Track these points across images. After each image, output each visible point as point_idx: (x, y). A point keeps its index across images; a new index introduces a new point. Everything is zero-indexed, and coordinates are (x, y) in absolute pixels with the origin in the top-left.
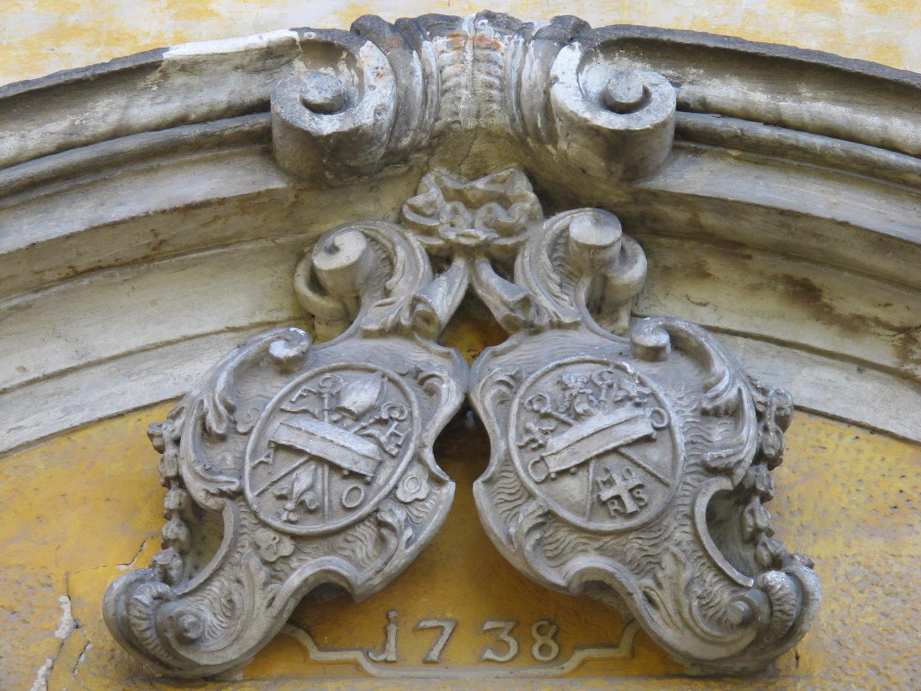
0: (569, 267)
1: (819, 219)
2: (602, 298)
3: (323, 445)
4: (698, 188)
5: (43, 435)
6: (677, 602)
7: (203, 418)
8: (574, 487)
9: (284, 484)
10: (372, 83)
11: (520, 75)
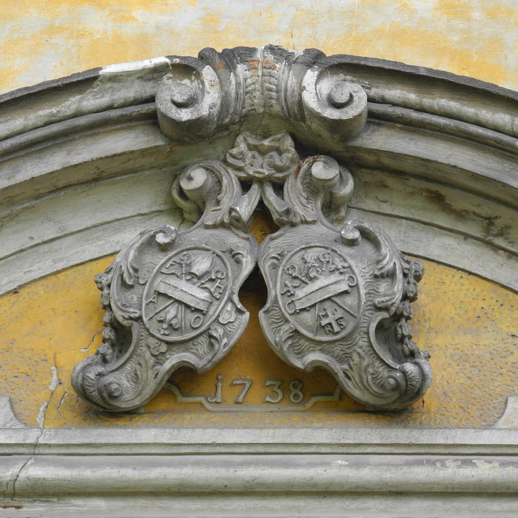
0: (312, 188)
1: (441, 163)
2: (331, 202)
3: (182, 294)
4: (379, 146)
5: (42, 275)
6: (361, 377)
7: (122, 275)
8: (308, 317)
9: (162, 314)
10: (208, 90)
11: (286, 84)
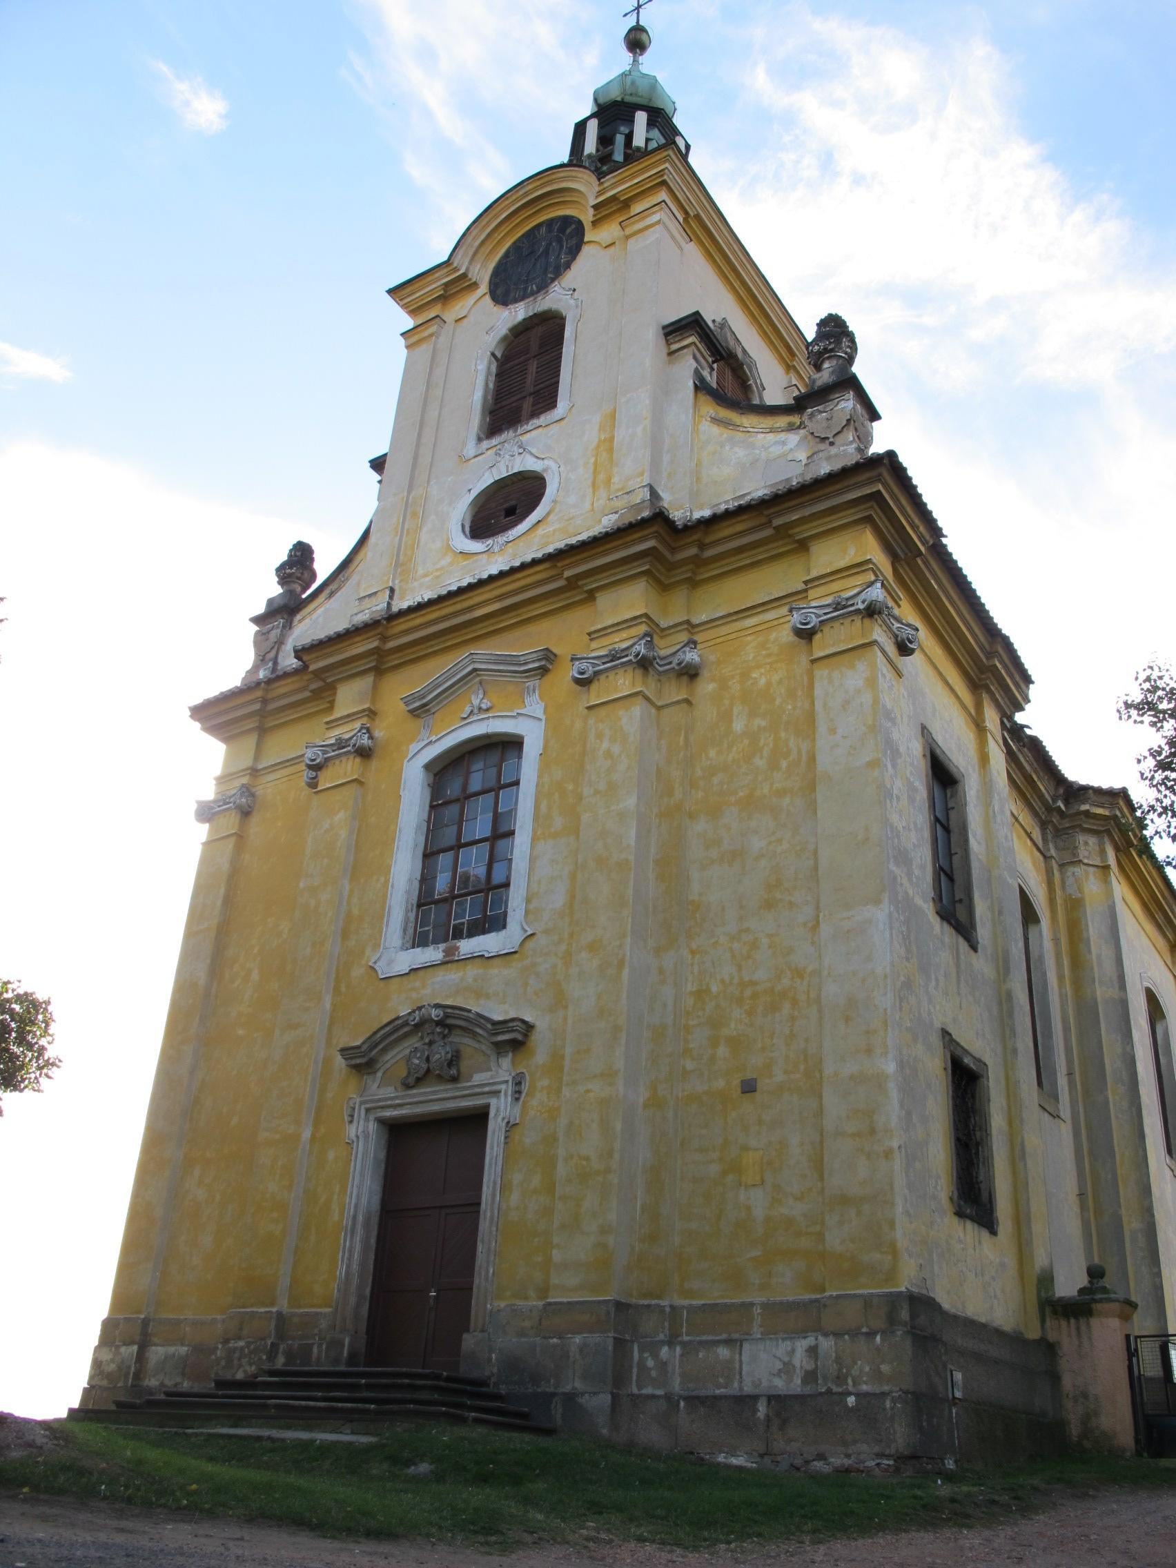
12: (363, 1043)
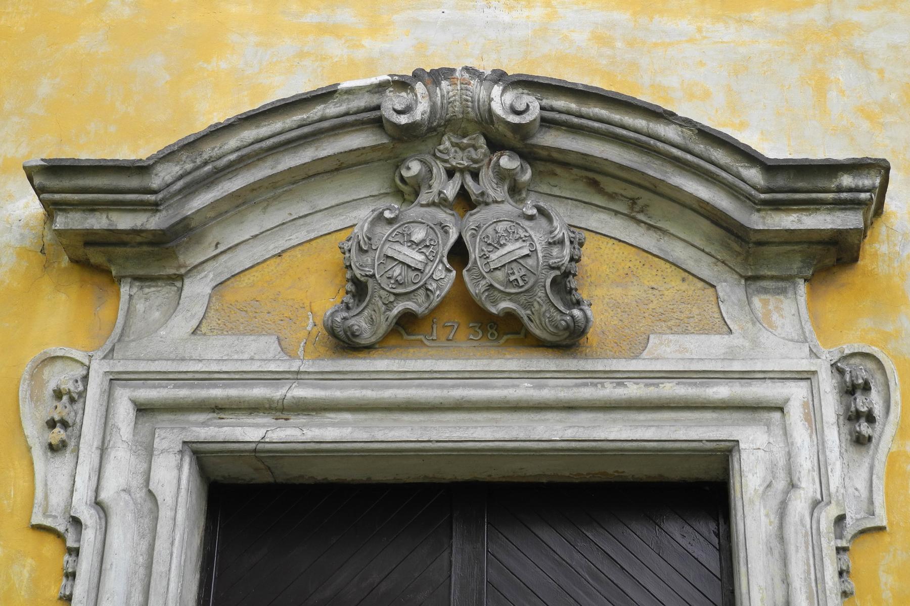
6: (540, 319)
7: (359, 243)
8: (500, 274)
9: (390, 272)
12: (168, 156)
